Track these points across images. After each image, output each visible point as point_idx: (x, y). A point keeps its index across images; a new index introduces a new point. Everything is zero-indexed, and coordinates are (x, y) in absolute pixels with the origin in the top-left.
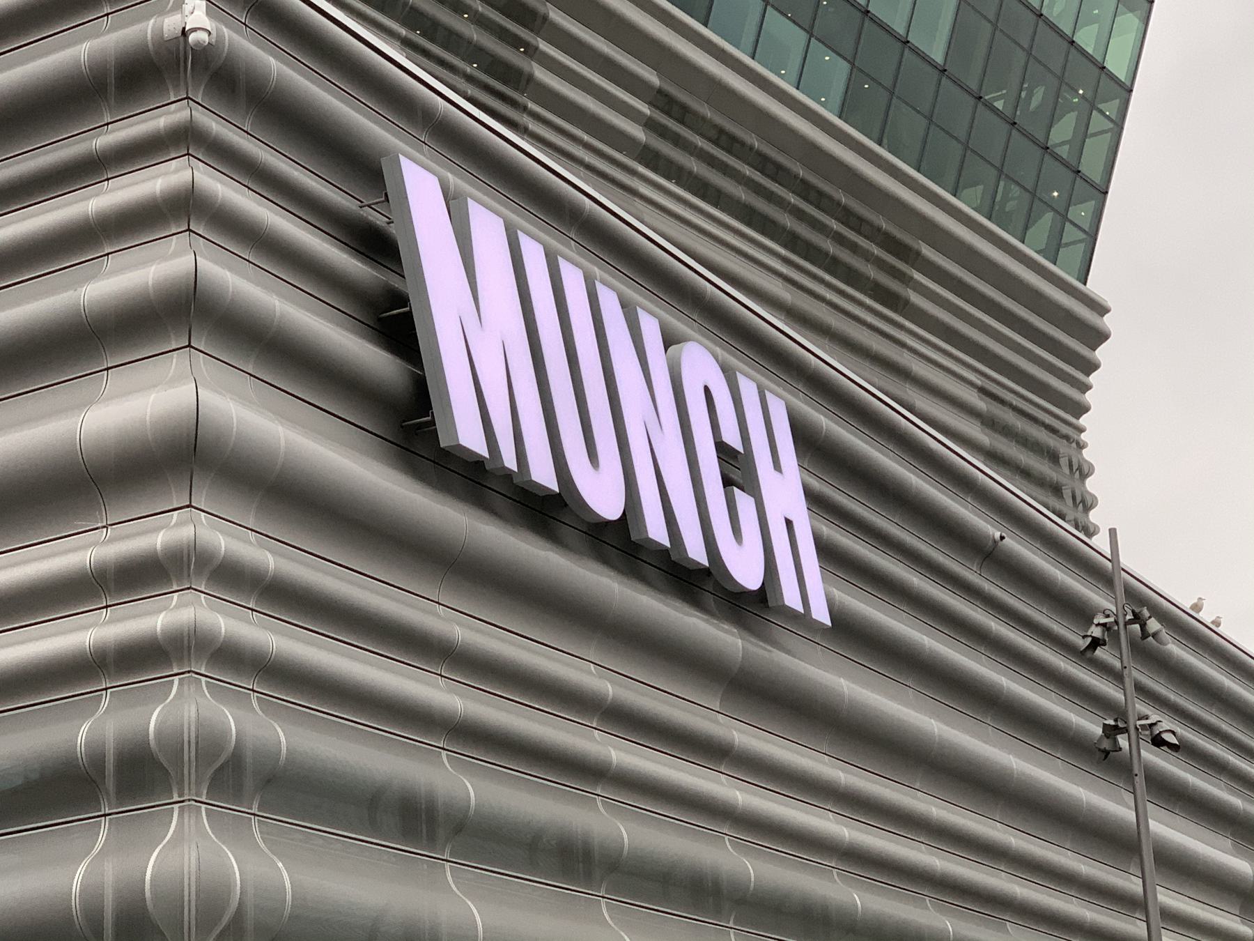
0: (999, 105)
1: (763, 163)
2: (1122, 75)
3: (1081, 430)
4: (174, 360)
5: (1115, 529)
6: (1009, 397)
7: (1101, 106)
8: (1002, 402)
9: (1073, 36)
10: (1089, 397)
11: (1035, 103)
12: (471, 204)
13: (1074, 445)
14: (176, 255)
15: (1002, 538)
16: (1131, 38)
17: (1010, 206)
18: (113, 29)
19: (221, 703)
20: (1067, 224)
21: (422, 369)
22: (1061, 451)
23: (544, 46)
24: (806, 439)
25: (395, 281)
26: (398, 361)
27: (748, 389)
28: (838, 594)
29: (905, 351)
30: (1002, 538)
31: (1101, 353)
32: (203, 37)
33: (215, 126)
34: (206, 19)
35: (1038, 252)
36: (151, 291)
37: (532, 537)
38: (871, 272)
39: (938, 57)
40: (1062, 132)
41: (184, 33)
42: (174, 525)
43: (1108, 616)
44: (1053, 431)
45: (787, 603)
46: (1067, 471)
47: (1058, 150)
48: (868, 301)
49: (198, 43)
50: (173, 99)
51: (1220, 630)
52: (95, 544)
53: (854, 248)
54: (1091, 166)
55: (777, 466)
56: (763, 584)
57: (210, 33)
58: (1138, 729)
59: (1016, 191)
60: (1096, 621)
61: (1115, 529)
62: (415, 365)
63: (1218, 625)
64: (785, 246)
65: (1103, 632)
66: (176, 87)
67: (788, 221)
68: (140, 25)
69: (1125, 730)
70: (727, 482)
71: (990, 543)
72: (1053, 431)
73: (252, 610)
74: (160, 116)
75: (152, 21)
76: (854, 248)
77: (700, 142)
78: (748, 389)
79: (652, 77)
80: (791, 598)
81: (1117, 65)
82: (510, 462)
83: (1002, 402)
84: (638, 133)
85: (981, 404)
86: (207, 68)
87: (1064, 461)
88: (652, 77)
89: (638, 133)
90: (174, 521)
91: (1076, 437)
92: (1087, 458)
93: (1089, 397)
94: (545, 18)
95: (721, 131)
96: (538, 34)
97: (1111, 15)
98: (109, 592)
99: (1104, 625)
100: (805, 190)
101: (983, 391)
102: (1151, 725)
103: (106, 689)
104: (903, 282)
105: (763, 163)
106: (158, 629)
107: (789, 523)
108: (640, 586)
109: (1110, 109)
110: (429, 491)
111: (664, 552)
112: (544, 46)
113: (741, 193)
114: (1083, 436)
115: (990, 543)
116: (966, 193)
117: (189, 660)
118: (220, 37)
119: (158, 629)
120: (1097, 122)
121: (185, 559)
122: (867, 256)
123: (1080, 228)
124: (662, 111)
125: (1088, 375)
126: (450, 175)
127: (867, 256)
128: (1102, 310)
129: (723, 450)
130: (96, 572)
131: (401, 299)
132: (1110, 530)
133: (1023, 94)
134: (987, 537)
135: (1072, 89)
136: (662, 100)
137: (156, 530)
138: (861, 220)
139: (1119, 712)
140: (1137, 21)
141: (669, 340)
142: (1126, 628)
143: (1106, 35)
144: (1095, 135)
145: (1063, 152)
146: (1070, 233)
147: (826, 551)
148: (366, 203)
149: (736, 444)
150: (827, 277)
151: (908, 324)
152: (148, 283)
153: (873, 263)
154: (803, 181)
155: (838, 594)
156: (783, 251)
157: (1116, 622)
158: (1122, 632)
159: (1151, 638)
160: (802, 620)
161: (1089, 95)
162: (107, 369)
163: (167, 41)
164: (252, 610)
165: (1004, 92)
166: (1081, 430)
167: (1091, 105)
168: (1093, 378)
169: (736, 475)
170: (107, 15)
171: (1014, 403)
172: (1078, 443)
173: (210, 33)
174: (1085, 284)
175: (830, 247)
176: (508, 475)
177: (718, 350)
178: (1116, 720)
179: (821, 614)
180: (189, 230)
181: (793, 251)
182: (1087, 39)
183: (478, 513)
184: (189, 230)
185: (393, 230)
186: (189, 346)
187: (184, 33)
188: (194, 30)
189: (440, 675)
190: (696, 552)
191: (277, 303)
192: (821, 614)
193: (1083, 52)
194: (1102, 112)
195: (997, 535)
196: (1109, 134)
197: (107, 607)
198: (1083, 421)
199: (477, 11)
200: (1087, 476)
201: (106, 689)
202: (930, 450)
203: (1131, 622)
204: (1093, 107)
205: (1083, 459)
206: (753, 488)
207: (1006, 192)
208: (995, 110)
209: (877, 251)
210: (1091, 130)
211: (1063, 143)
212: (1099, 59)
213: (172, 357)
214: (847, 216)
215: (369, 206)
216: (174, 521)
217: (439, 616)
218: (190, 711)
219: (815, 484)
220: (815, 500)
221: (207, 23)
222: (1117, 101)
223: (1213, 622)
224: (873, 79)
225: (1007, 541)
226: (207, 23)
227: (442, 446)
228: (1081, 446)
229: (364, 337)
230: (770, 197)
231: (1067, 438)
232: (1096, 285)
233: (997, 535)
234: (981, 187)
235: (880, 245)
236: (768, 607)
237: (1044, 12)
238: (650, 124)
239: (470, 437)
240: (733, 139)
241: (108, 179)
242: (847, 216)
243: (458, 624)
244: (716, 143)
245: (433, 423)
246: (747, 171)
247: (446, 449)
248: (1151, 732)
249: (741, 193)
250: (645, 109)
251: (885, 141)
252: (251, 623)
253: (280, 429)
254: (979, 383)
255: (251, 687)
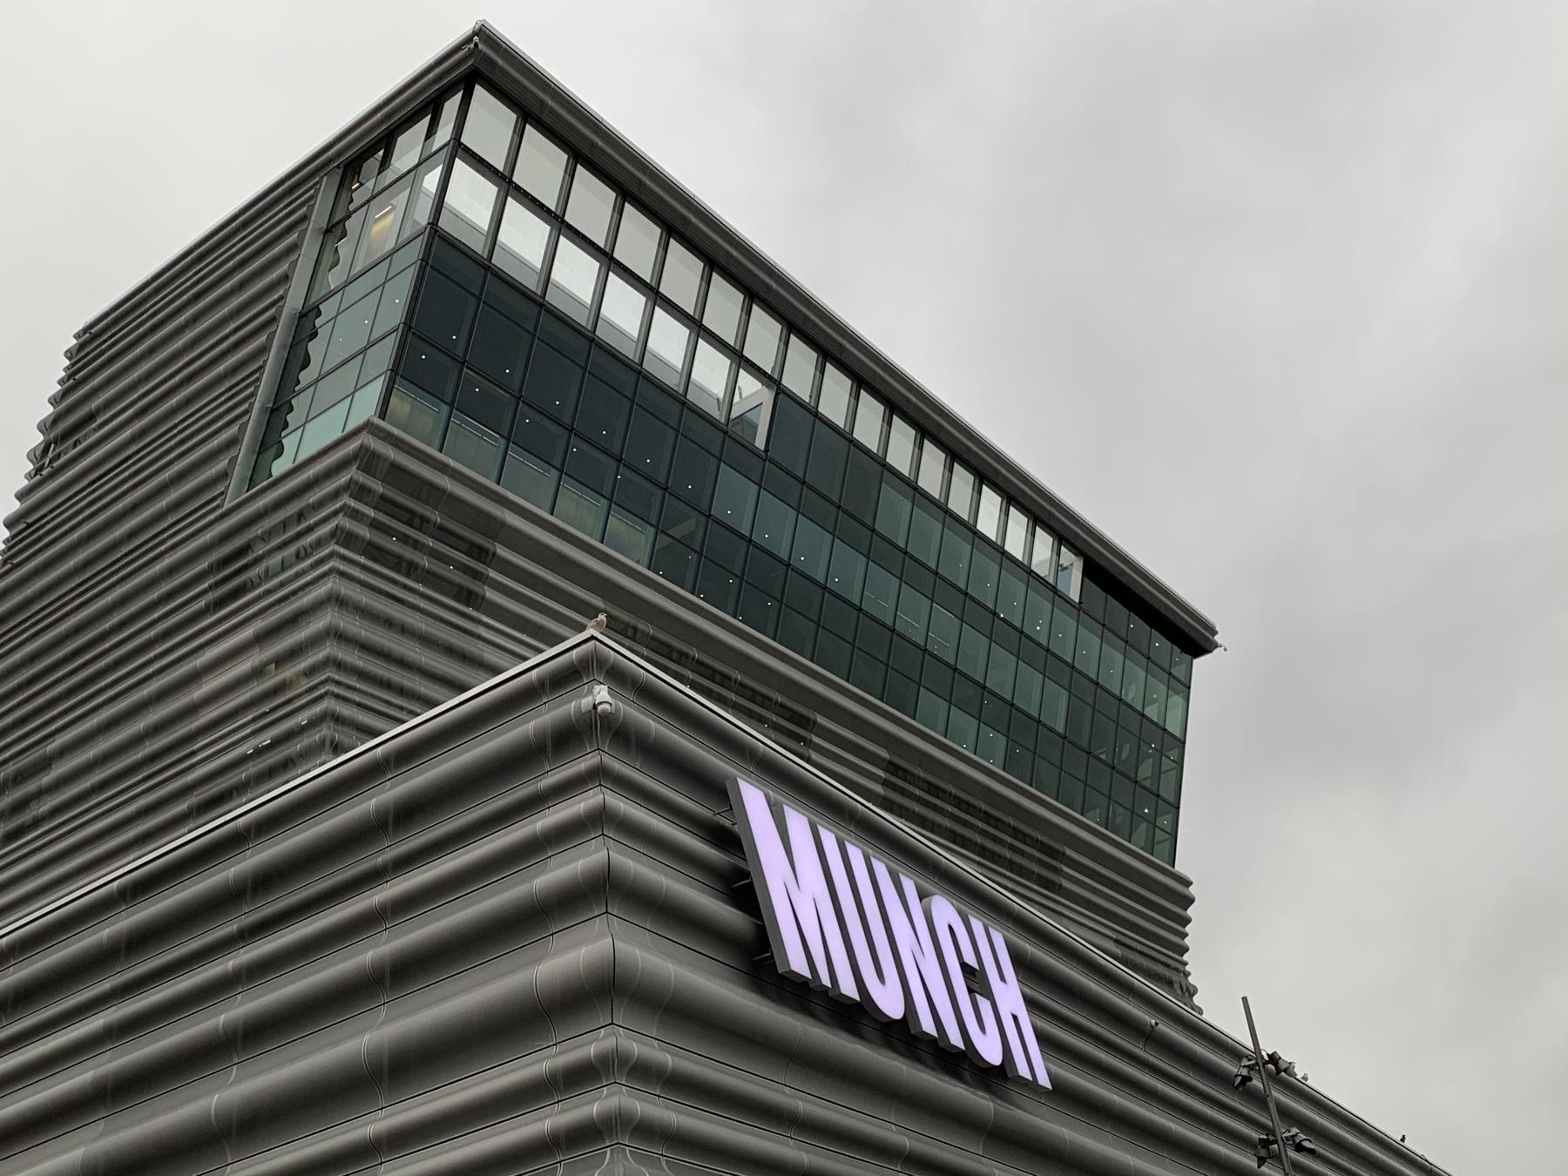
0: (1103, 757)
1: (958, 802)
2: (1177, 733)
3: (1185, 964)
4: (598, 923)
5: (1246, 998)
6: (1134, 944)
7: (1168, 754)
8: (1131, 948)
9: (1143, 710)
10: (1187, 941)
11: (1124, 756)
12: (785, 807)
13: (1182, 974)
14: (597, 851)
15: (1157, 1024)
16: (1180, 711)
17: (1118, 820)
18: (550, 710)
19: (640, 1164)
20: (1157, 830)
21: (763, 921)
22: (1174, 979)
23: (816, 739)
24: (1019, 960)
25: (741, 863)
26: (746, 916)
27: (977, 926)
28: (1054, 1068)
29: (1063, 918)
30: (1157, 1024)
31: (1191, 912)
32: (607, 706)
33: (616, 765)
34: (609, 696)
35: (1141, 849)
36: (579, 875)
37: (845, 1035)
38: (1035, 868)
39: (1061, 729)
40: (1145, 771)
41: (595, 707)
42: (606, 1097)
43: (1250, 1060)
44: (1168, 966)
45: (1020, 1074)
46: (1179, 992)
47: (1144, 783)
48: (1035, 887)
49: (604, 711)
50: (589, 751)
51: (1308, 1083)
52: (548, 1058)
53: (1022, 853)
54: (1166, 792)
55: (1003, 979)
56: (1003, 1061)
57: (611, 704)
58: (1283, 1141)
59: (1121, 810)
60: (1243, 1064)
61: (1246, 998)
62: (756, 919)
63: (1306, 1080)
64: (979, 855)
65: (1249, 1072)
66: (591, 743)
67: (979, 839)
68: (565, 707)
69: (1275, 1142)
70: (971, 991)
71: (1149, 1027)
72: (1168, 966)
73: (658, 1096)
74: (581, 763)
75: (573, 703)
76: (1022, 853)
77: (918, 792)
78: (977, 926)
79: (884, 754)
80: (1023, 1071)
81: (1173, 727)
82: (826, 980)
83: (1131, 948)
84: (879, 789)
85: (1118, 951)
86: (610, 729)
87: (1176, 986)
88: (884, 754)
89: (879, 789)
90: (602, 1036)
91: (1182, 969)
92: (1192, 983)
93: (1187, 941)
94: (815, 722)
95: (930, 784)
96: (811, 731)
97: (1164, 698)
98: (560, 1092)
99: (1248, 1066)
100: (987, 818)
101: (1117, 941)
102: (1293, 1136)
103: (560, 1162)
104: (1056, 873)
105: (958, 802)
106: (592, 1055)
107: (1015, 1018)
108: (920, 1067)
109: (1173, 755)
110: (773, 1005)
111: (932, 1040)
112: (816, 739)
113: (947, 823)
114: (1187, 968)
115: (1149, 1027)
116: (1091, 814)
117: (617, 1135)
118: (618, 710)
119: (592, 1055)
120: (1166, 762)
121: (614, 1122)
122: (1032, 858)
123: (1166, 832)
124: (892, 774)
125: (1184, 927)
126: (770, 792)
127: (1032, 858)
128: (1188, 883)
129: (965, 967)
130: (541, 994)
131: (747, 875)
132: (1243, 998)
133: (1117, 749)
134: (1146, 1024)
135: (1147, 743)
136: (891, 767)
137: (590, 1043)
138: (1024, 834)
139: (1270, 1131)
140: (1181, 700)
141: (923, 895)
142: (1264, 1067)
143: (1163, 708)
144: (1166, 772)
145: (1147, 784)
146: (1160, 835)
147: (1043, 1038)
148: (717, 812)
149: (975, 965)
150: (1008, 873)
151: (485, 619)
152: (570, 712)
153: (1036, 862)
154: (985, 812)
155: (1054, 1068)
156: (977, 858)
157: (1257, 1064)
158: (1262, 1069)
159: (1283, 1073)
160: (1031, 1085)
161: (1159, 748)
162: (552, 934)
163: (584, 714)
164: (658, 1096)
165: (1104, 749)
166: (1185, 964)
167: (1161, 752)
168: (1188, 929)
169: (975, 987)
170: (545, 703)
171: (1139, 948)
172: (1184, 973)
173: (611, 704)
174: (1174, 867)
175: (1008, 854)
176: (825, 990)
177: (954, 902)
178: (1267, 1135)
179: (1044, 1081)
180: (603, 834)
181: (984, 857)
182: (1152, 712)
183: (807, 1019)
184: (603, 834)
185: (736, 828)
186: (607, 912)
187: (595, 707)
188: (601, 703)
189: (790, 1137)
190: (956, 1039)
191: (664, 880)
192: (1044, 1081)
193: (1152, 721)
194: (1167, 757)
195: (1153, 1022)
196: (1175, 771)
197: (558, 1102)
198: (1186, 957)
199: (772, 721)
200: (1194, 995)
201: (560, 1162)
202: (1100, 964)
203: (1267, 1062)
204: (1162, 753)
205: (1190, 984)
206: (989, 996)
207: (1114, 812)
208: (1100, 760)
209: (1037, 854)
210: (1163, 769)
211: (1146, 779)
212: (1162, 725)
213: (595, 922)
214: (1016, 833)
215: (719, 814)
216: (602, 1036)
217: (785, 1094)
218: (619, 1172)
219: (1028, 991)
220: (1030, 1003)
221: (609, 699)
222: (1176, 750)
223: (1302, 1078)
224: (1021, 745)
225: (1160, 1026)
226: (609, 699)
227: (780, 972)
228: (1187, 975)
229: (724, 901)
230: (965, 824)
231: (1176, 969)
232: (1180, 867)
233: (1153, 1022)
234: (1098, 811)
235: (1039, 850)
236: (1008, 1078)
237: (1122, 697)
238: (885, 783)
239: (798, 965)
240: (937, 788)
241: (548, 808)
242: (1016, 833)
243: (800, 1099)
244: (928, 792)
245: (772, 957)
246: (950, 809)
247: (784, 975)
248: (1294, 1141)
249: (947, 823)
250: (882, 774)
251: (1034, 784)
252: (658, 1106)
253: (671, 966)
254: (1114, 936)
255: (660, 1153)
